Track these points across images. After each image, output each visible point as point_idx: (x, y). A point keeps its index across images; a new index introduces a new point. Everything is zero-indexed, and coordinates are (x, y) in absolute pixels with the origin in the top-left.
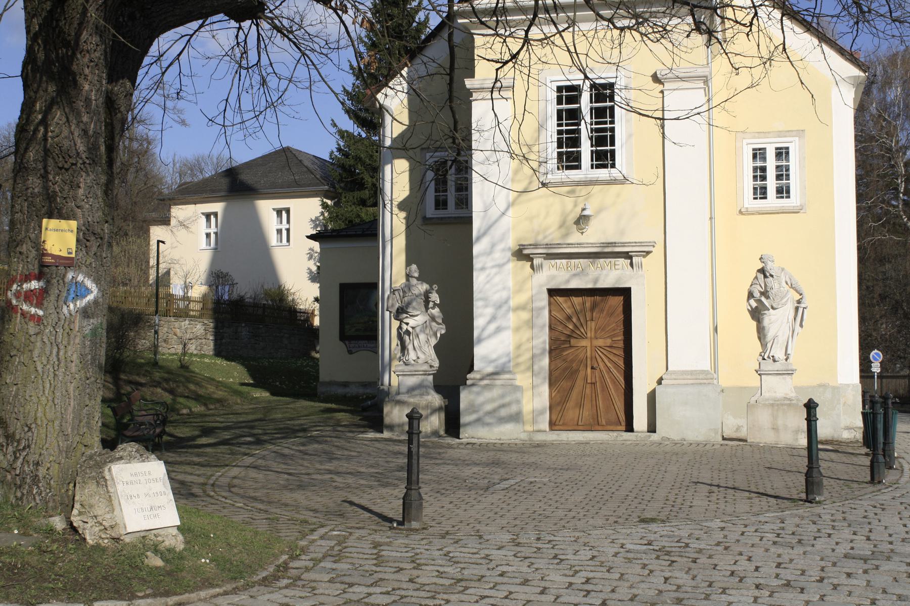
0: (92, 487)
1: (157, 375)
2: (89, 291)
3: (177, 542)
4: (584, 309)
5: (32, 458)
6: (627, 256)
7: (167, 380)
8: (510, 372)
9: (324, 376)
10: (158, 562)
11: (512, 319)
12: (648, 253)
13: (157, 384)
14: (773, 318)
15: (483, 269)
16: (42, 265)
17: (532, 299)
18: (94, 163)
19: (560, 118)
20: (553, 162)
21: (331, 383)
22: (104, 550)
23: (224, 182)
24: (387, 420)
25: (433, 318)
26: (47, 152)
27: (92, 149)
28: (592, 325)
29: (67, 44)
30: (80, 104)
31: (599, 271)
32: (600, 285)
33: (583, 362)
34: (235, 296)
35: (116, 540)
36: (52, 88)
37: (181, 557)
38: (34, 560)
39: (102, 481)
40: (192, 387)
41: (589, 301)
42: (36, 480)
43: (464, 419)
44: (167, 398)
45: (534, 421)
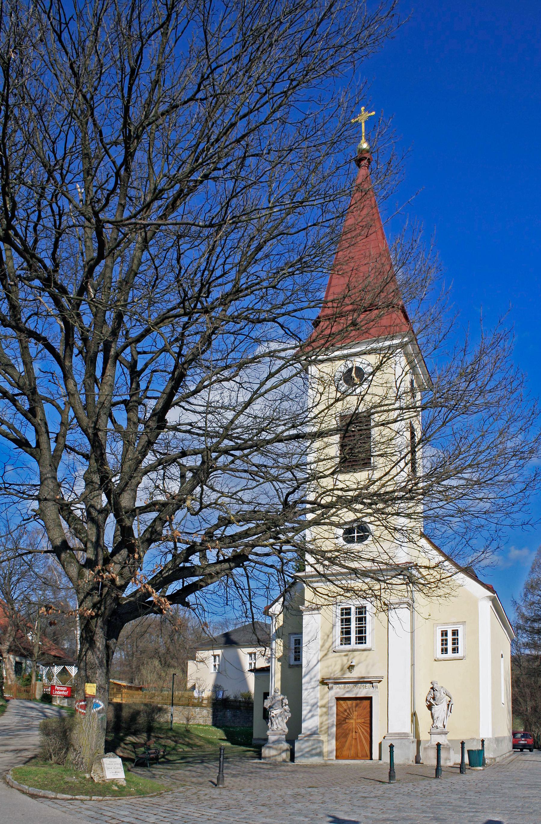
0: (97, 765)
1: (170, 734)
2: (100, 706)
3: (124, 783)
4: (352, 707)
5: (81, 756)
6: (370, 682)
7: (174, 736)
8: (317, 734)
9: (255, 736)
10: (116, 788)
11: (319, 711)
12: (380, 681)
13: (169, 738)
14: (436, 709)
15: (306, 689)
16: (85, 697)
17: (328, 702)
18: (101, 666)
19: (342, 622)
20: (338, 642)
21: (259, 739)
22: (100, 784)
23: (223, 640)
24: (263, 755)
25: (285, 711)
26: (86, 664)
27: (101, 662)
28: (356, 713)
29: (92, 632)
30: (96, 650)
31: (358, 690)
32: (358, 696)
33: (351, 730)
34: (225, 697)
35: (104, 781)
36: (88, 645)
37: (124, 787)
38: (78, 785)
39: (100, 764)
40: (187, 740)
41: (354, 702)
42: (82, 763)
43: (296, 755)
44: (173, 744)
45: (328, 756)
